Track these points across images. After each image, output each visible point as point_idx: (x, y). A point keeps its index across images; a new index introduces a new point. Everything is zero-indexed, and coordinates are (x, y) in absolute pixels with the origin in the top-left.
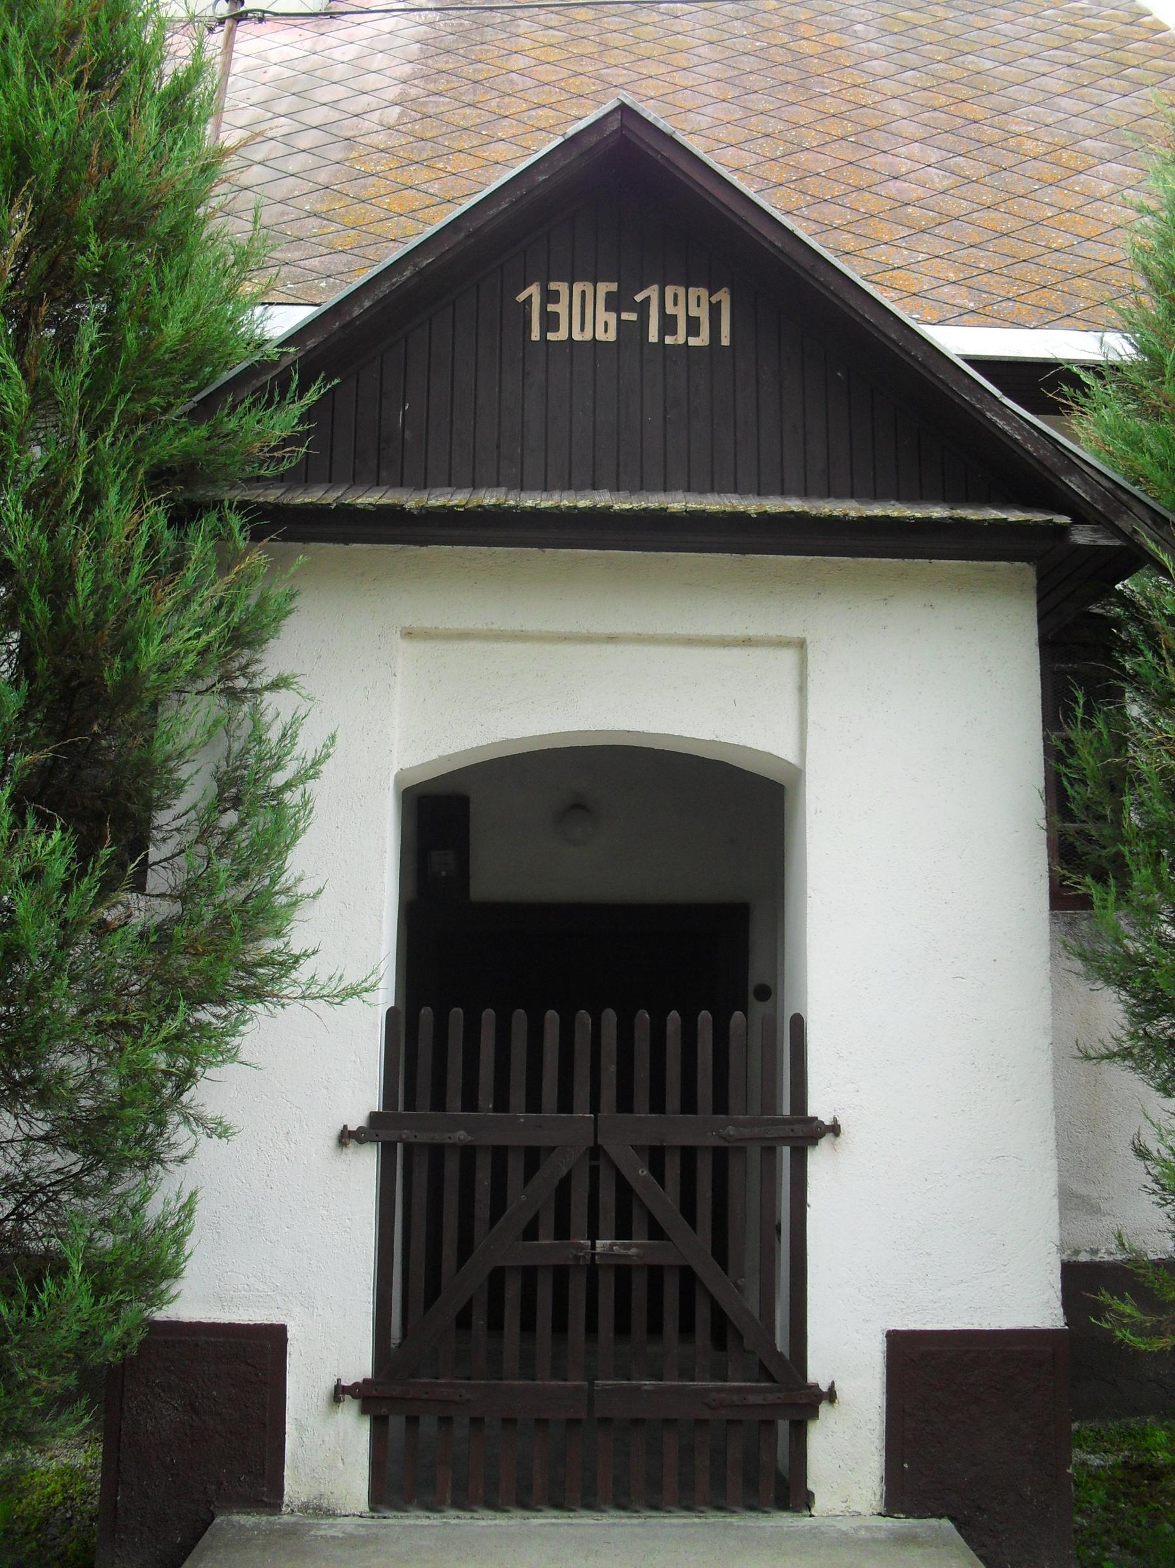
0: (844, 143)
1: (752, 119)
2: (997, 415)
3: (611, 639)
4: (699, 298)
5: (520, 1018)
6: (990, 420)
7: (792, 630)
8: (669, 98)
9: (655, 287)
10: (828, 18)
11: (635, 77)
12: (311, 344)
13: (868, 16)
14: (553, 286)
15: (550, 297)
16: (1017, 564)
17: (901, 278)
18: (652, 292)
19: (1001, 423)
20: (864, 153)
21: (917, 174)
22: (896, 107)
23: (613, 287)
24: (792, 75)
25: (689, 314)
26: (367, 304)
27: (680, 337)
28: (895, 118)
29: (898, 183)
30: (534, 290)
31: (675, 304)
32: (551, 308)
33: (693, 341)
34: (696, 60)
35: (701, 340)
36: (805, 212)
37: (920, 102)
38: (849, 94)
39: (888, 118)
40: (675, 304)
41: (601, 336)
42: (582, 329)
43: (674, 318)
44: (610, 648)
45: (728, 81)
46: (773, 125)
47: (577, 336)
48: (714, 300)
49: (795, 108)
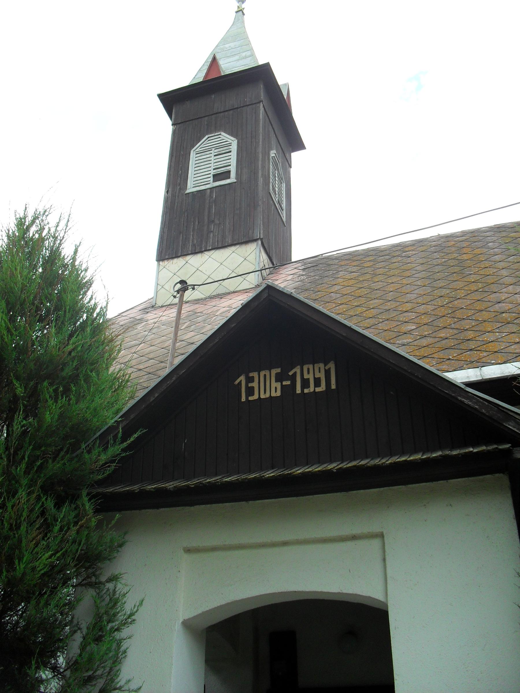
0: (476, 293)
1: (435, 292)
2: (464, 398)
3: (285, 544)
4: (320, 368)
6: (461, 401)
7: (375, 528)
8: (399, 290)
9: (299, 367)
10: (477, 243)
11: (385, 284)
12: (132, 416)
13: (495, 238)
14: (251, 375)
16: (497, 475)
17: (492, 346)
18: (297, 370)
19: (466, 401)
20: (486, 294)
21: (510, 299)
22: (504, 273)
23: (279, 370)
24: (457, 269)
25: (315, 377)
26: (156, 395)
27: (312, 389)
28: (502, 277)
29: (500, 305)
30: (242, 378)
31: (308, 373)
32: (250, 385)
33: (318, 390)
34: (414, 272)
35: (322, 388)
36: (453, 326)
37: (515, 268)
38: (482, 272)
39: (499, 278)
40: (308, 373)
41: (274, 394)
42: (265, 392)
43: (308, 380)
44: (285, 548)
45: (428, 278)
46: (444, 292)
47: (263, 396)
48: (327, 368)
49: (456, 282)
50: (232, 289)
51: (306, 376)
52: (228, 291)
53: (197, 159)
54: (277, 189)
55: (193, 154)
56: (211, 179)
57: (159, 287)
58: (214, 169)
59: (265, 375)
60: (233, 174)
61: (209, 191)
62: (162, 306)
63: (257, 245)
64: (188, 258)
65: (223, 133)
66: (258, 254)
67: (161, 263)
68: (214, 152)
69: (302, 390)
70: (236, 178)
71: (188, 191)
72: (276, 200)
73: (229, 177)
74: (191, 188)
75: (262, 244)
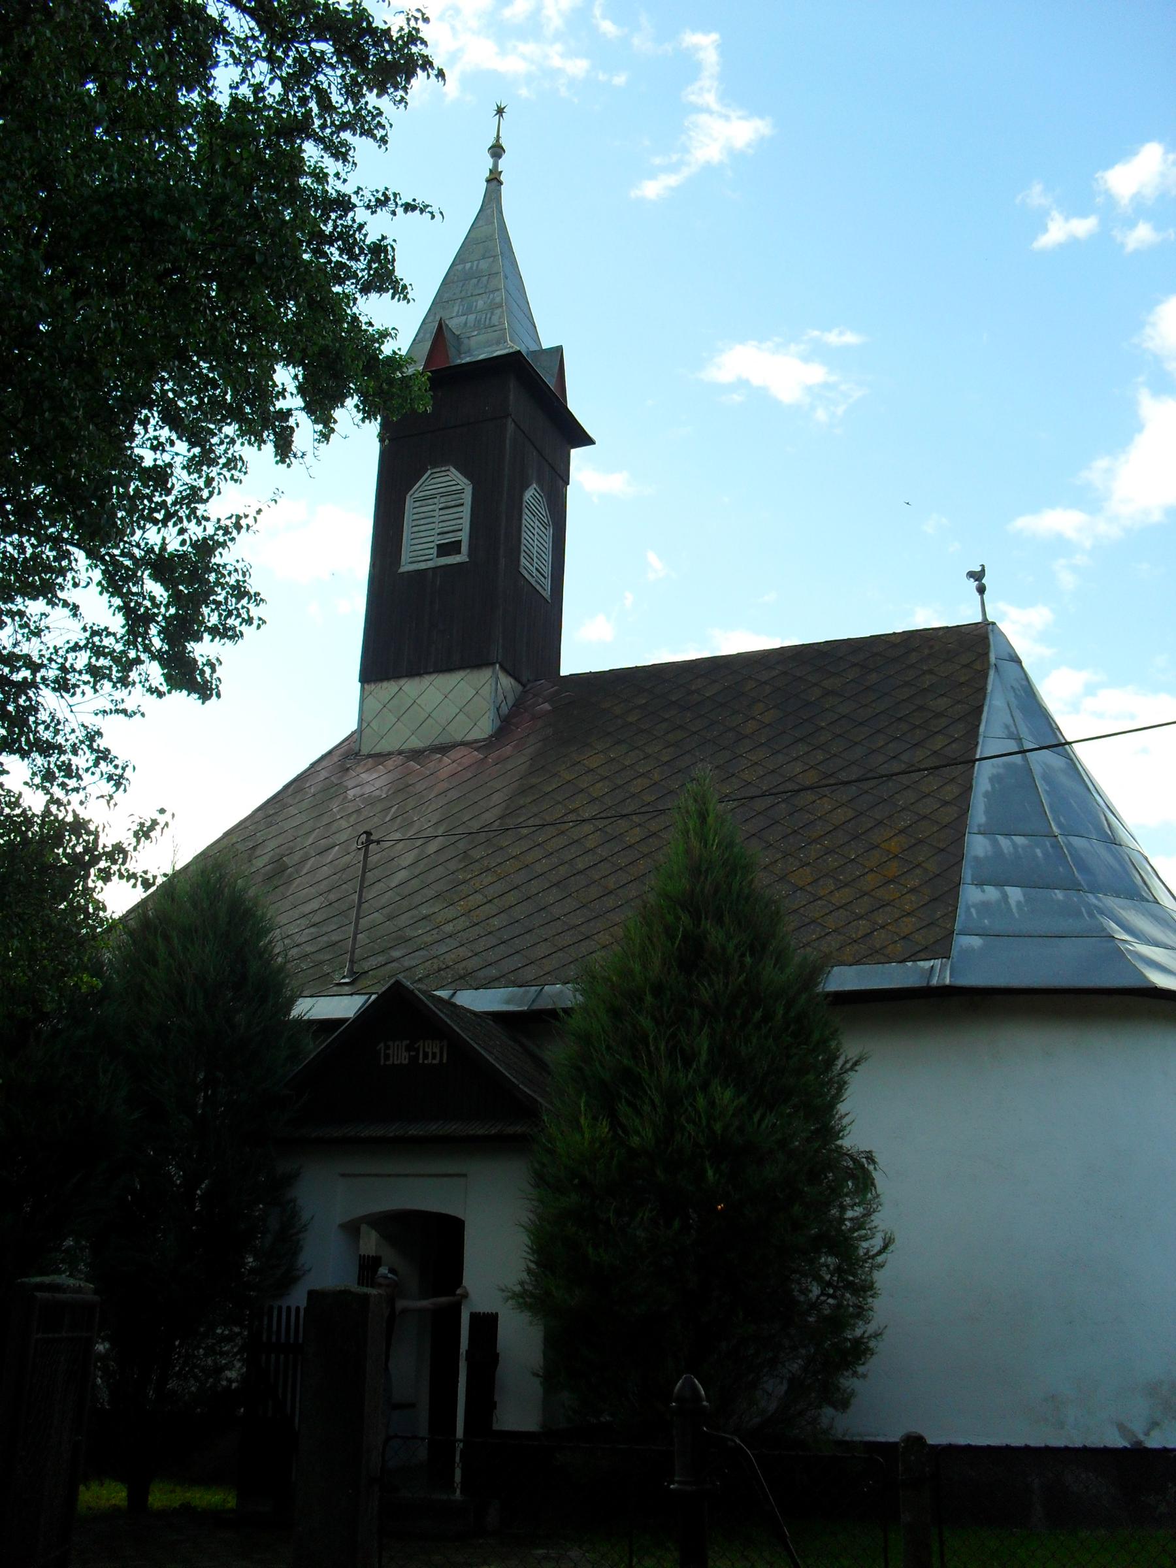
5: (283, 1340)
15: (387, 1047)
18: (421, 1043)
25: (433, 1052)
30: (382, 1045)
35: (436, 1062)
56: (434, 551)
57: (365, 725)
60: (464, 548)
61: (430, 573)
62: (370, 756)
64: (402, 682)
65: (453, 469)
67: (366, 686)
68: (441, 501)
70: (469, 556)
71: (402, 570)
73: (459, 552)
75: (502, 667)
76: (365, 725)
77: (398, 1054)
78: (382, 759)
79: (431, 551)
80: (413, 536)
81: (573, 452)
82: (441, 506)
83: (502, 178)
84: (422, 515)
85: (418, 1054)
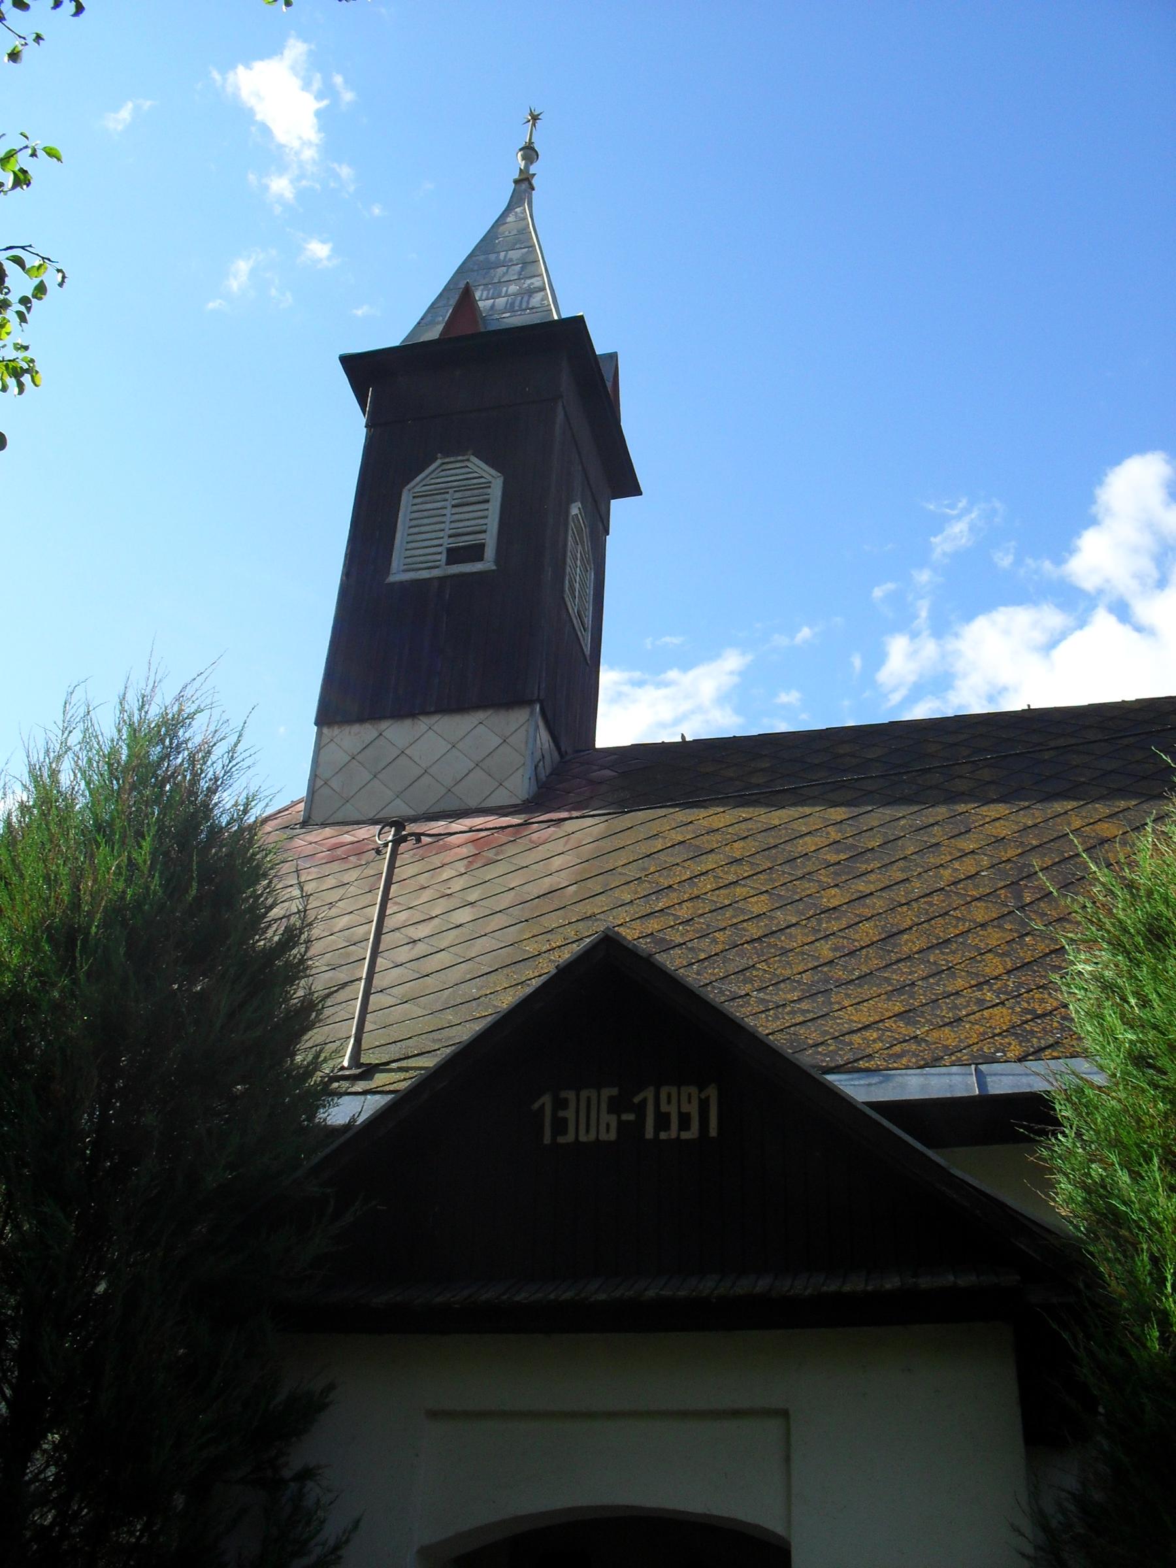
9: (652, 1089)
14: (564, 1094)
18: (649, 1094)
23: (614, 1091)
25: (681, 1110)
27: (673, 1134)
30: (546, 1099)
31: (669, 1102)
32: (561, 1114)
33: (685, 1135)
35: (692, 1134)
40: (669, 1102)
41: (603, 1137)
42: (588, 1131)
43: (668, 1115)
47: (583, 1138)
48: (703, 1096)
50: (473, 803)
51: (664, 1108)
52: (463, 807)
53: (415, 508)
54: (577, 586)
55: (406, 497)
56: (443, 557)
57: (319, 783)
58: (450, 536)
59: (589, 1099)
60: (490, 552)
63: (532, 713)
64: (384, 725)
66: (531, 730)
67: (325, 730)
68: (452, 497)
69: (656, 1134)
70: (497, 561)
72: (573, 610)
73: (481, 558)
74: (398, 574)
75: (542, 709)
76: (319, 783)
77: (591, 1119)
78: (347, 828)
79: (438, 557)
80: (410, 538)
81: (612, 502)
82: (454, 502)
83: (534, 182)
84: (426, 514)
85: (642, 1117)
